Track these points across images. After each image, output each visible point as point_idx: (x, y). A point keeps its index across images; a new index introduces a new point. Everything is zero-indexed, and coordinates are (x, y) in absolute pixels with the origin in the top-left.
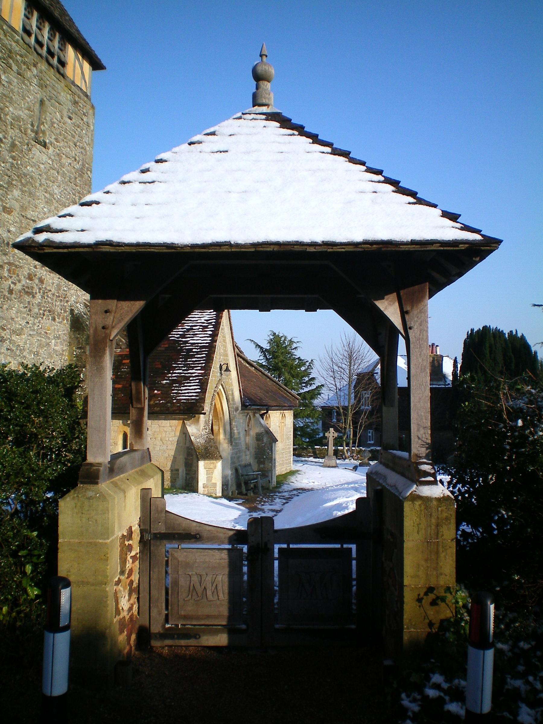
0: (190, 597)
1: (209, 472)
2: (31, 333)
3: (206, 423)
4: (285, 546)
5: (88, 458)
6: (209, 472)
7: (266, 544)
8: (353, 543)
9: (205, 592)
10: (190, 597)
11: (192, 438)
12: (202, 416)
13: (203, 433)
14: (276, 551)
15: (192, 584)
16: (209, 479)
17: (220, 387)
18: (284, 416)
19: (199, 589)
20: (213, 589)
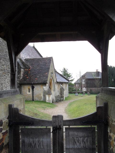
0: (29, 147)
1: (49, 98)
2: (7, 65)
3: (48, 86)
4: (68, 127)
5: (95, 99)
6: (49, 98)
7: (60, 126)
8: (96, 125)
9: (35, 145)
10: (29, 147)
11: (45, 89)
12: (47, 84)
13: (47, 88)
14: (64, 129)
15: (30, 142)
16: (49, 99)
17: (51, 77)
18: (66, 85)
19: (33, 145)
20: (39, 144)
